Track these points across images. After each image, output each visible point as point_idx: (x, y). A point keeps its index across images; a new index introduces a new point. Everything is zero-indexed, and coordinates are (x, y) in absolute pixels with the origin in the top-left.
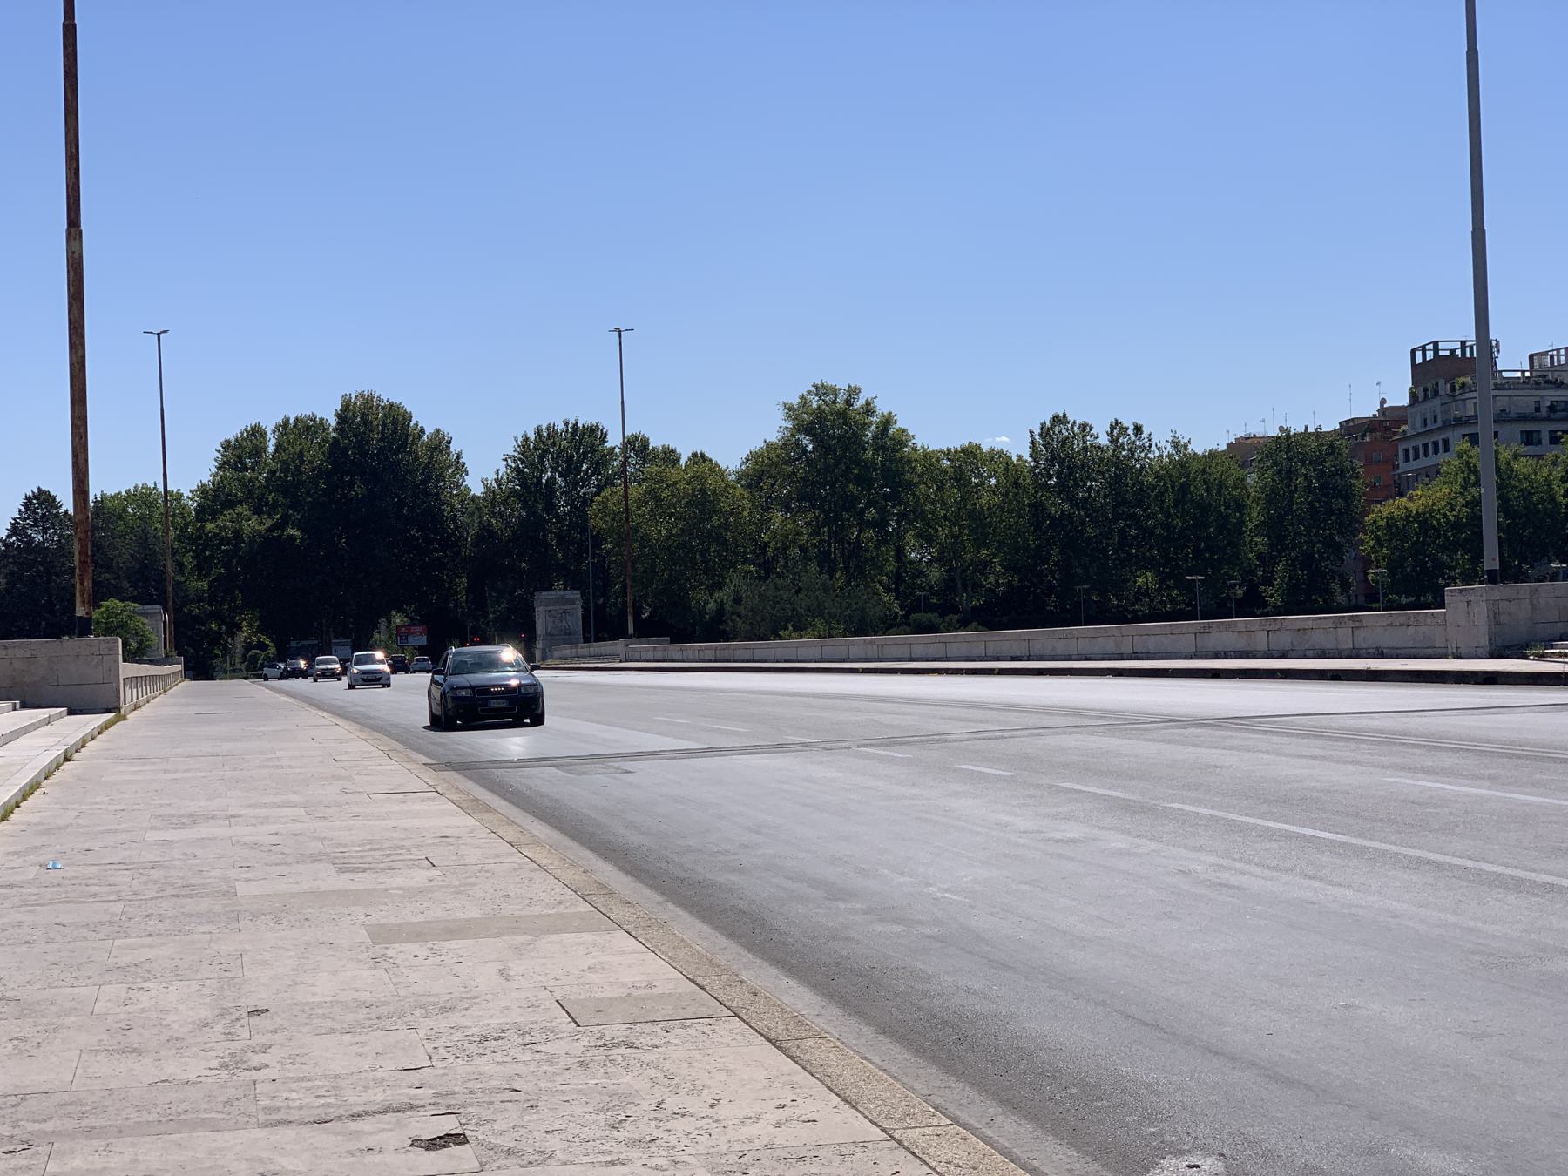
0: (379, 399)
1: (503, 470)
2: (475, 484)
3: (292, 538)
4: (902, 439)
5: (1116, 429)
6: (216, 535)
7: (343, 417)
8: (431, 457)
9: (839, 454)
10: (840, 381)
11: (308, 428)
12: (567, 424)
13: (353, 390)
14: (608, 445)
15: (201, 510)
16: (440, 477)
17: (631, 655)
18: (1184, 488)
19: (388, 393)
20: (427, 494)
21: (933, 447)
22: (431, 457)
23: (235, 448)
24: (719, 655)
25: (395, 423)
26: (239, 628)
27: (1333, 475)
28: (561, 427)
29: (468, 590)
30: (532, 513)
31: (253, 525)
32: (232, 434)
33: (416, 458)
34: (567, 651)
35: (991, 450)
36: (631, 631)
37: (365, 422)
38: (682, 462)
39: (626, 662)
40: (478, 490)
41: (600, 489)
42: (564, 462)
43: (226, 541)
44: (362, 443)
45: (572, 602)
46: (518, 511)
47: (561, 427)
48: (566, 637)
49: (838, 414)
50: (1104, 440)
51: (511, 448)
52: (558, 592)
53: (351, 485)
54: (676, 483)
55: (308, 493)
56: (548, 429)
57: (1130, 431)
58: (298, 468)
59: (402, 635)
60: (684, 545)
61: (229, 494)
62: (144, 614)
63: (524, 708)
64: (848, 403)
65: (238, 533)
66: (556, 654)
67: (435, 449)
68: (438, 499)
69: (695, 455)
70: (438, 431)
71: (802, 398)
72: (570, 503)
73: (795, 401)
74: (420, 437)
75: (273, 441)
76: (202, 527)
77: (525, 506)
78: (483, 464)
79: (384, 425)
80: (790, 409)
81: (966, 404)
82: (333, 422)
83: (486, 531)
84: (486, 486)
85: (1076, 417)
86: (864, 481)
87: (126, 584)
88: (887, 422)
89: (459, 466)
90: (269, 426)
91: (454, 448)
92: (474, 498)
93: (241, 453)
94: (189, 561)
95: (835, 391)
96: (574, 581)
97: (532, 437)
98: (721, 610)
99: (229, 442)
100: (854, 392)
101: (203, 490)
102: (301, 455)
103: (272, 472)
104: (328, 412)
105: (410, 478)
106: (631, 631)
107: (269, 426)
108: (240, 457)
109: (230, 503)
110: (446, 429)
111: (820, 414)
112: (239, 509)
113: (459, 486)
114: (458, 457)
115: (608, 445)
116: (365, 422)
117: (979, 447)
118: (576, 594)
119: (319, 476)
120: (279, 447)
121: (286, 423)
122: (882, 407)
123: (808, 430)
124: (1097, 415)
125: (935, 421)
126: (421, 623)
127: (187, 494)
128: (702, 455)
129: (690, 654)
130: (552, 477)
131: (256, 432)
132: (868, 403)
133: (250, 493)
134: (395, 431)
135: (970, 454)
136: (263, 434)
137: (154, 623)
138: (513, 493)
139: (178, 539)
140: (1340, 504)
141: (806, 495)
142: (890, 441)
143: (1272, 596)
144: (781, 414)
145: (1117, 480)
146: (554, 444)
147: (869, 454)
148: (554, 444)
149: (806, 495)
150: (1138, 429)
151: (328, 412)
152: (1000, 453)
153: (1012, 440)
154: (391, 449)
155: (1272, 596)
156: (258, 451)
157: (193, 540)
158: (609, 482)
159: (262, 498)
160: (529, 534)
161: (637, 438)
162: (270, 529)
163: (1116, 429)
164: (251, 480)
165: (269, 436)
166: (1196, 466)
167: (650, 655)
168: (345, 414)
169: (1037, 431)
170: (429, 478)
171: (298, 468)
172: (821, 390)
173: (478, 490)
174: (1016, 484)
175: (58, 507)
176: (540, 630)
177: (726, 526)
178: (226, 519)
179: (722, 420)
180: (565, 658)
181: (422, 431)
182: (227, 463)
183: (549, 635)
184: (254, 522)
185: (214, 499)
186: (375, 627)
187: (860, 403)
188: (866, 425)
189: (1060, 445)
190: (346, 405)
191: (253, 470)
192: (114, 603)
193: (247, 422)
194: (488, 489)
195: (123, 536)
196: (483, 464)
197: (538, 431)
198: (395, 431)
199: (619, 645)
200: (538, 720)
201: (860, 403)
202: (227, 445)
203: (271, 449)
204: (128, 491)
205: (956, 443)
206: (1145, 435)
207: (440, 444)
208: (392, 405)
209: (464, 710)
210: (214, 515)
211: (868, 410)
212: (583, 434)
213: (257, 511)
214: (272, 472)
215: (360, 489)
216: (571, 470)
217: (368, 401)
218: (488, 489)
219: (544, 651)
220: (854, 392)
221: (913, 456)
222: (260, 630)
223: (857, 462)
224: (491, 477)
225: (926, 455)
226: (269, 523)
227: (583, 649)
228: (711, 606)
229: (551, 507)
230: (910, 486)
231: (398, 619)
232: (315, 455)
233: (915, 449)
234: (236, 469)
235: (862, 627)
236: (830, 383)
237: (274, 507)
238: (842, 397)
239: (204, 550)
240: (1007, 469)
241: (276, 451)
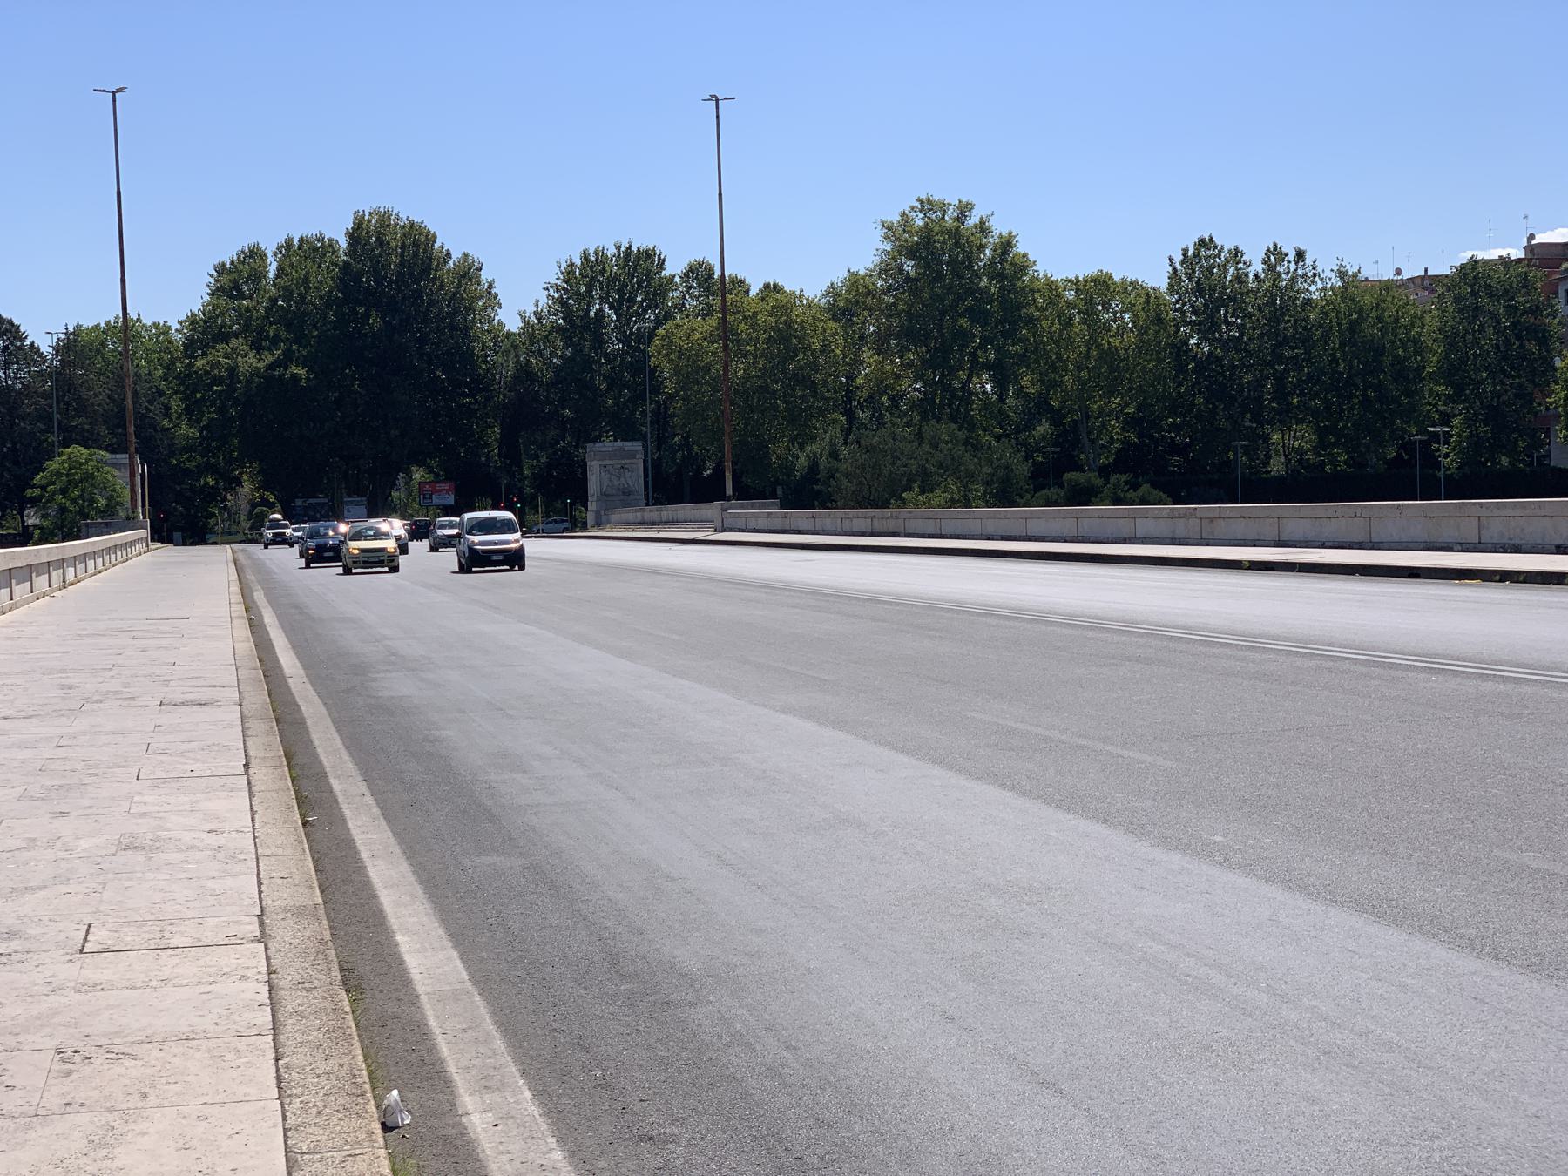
0: (398, 218)
1: (544, 301)
2: (510, 319)
3: (295, 378)
4: (1022, 265)
5: (1275, 255)
6: (207, 373)
7: (355, 236)
8: (459, 285)
9: (949, 284)
10: (951, 196)
11: (316, 249)
12: (618, 248)
13: (366, 208)
14: (666, 273)
15: (190, 344)
16: (470, 309)
17: (730, 522)
18: (1354, 327)
19: (408, 209)
20: (453, 328)
21: (1058, 276)
22: (459, 285)
23: (230, 272)
24: (878, 526)
25: (416, 244)
26: (239, 482)
27: (1525, 312)
28: (611, 251)
29: (501, 443)
30: (578, 350)
31: (251, 362)
32: (228, 255)
33: (442, 287)
34: (630, 514)
35: (1124, 280)
36: (729, 491)
37: (380, 242)
38: (753, 293)
39: (721, 535)
40: (513, 325)
41: (659, 323)
42: (615, 292)
43: (218, 380)
44: (377, 270)
45: (632, 455)
46: (559, 351)
47: (611, 251)
48: (623, 498)
49: (949, 232)
50: (1257, 267)
51: (553, 276)
52: (607, 445)
53: (367, 316)
54: (756, 313)
55: (315, 326)
56: (596, 253)
57: (1291, 257)
58: (302, 297)
59: (426, 492)
60: (764, 389)
61: (223, 325)
62: (114, 465)
63: (515, 560)
64: (960, 218)
65: (232, 371)
66: (615, 517)
67: (464, 275)
68: (467, 335)
69: (767, 286)
70: (466, 255)
71: (903, 215)
72: (625, 340)
73: (896, 219)
74: (445, 262)
75: (275, 265)
76: (191, 365)
77: (569, 342)
78: (519, 294)
79: (403, 246)
80: (889, 228)
81: (1098, 225)
82: (343, 243)
83: (524, 373)
84: (523, 319)
85: (1226, 242)
86: (977, 315)
87: (103, 430)
88: (1007, 244)
89: (492, 298)
90: (270, 247)
91: (485, 276)
92: (509, 335)
93: (236, 279)
94: (176, 404)
95: (943, 207)
96: (627, 431)
97: (578, 262)
98: (814, 467)
99: (224, 265)
100: (964, 209)
101: (192, 321)
102: (306, 280)
103: (274, 301)
104: (337, 232)
105: (434, 310)
106: (729, 491)
107: (270, 247)
108: (235, 282)
109: (223, 336)
110: (476, 254)
111: (927, 235)
112: (234, 342)
113: (490, 321)
114: (490, 286)
115: (666, 273)
116: (380, 242)
117: (1109, 276)
118: (636, 446)
119: (328, 305)
120: (281, 271)
121: (289, 244)
122: (999, 227)
123: (912, 253)
124: (1249, 239)
125: (1058, 254)
126: (447, 479)
127: (175, 326)
128: (775, 285)
129: (828, 524)
130: (601, 310)
131: (254, 254)
132: (982, 222)
133: (246, 328)
134: (416, 254)
135: (1101, 283)
136: (263, 256)
137: (123, 476)
138: (555, 328)
139: (164, 378)
140: (1533, 347)
141: (911, 334)
142: (1009, 266)
143: (1447, 456)
144: (879, 233)
145: (1277, 315)
146: (604, 270)
147: (984, 282)
148: (604, 270)
149: (911, 334)
150: (1300, 255)
151: (337, 232)
152: (1134, 284)
153: (1152, 271)
154: (411, 275)
155: (1447, 456)
156: (257, 276)
157: (182, 379)
158: (668, 316)
159: (261, 330)
160: (574, 375)
161: (700, 265)
162: (271, 367)
163: (1275, 255)
164: (248, 310)
165: (270, 259)
166: (1368, 301)
167: (762, 524)
168: (356, 236)
169: (1178, 258)
170: (456, 312)
171: (302, 297)
172: (927, 206)
173: (513, 325)
174: (1159, 320)
175: (21, 338)
176: (593, 486)
177: (814, 366)
178: (218, 354)
179: (808, 245)
180: (625, 524)
181: (448, 255)
182: (222, 289)
183: (604, 495)
184: (251, 359)
185: (205, 331)
186: (393, 485)
187: (973, 220)
188: (982, 247)
189: (1205, 275)
190: (359, 223)
191: (250, 297)
192: (77, 451)
193: (245, 243)
194: (527, 323)
195: (100, 373)
196: (519, 294)
197: (585, 256)
198: (416, 254)
199: (712, 510)
200: (522, 568)
201: (973, 220)
202: (221, 269)
203: (272, 274)
204: (107, 323)
205: (1083, 269)
206: (1309, 261)
207: (468, 271)
208: (412, 224)
209: (474, 561)
210: (205, 348)
211: (983, 228)
212: (638, 258)
213: (259, 350)
214: (274, 301)
215: (375, 321)
216: (623, 301)
217: (384, 218)
218: (527, 323)
219: (598, 514)
220: (964, 209)
221: (1037, 285)
222: (265, 486)
223: (971, 291)
224: (530, 310)
225: (1051, 285)
226: (269, 359)
227: (652, 512)
228: (802, 462)
229: (600, 343)
230: (1031, 321)
231: (418, 475)
232: (324, 282)
233: (1037, 278)
234: (232, 297)
235: (1004, 495)
236: (936, 198)
237: (275, 342)
238: (951, 213)
239: (195, 391)
240: (1147, 301)
241: (277, 276)
